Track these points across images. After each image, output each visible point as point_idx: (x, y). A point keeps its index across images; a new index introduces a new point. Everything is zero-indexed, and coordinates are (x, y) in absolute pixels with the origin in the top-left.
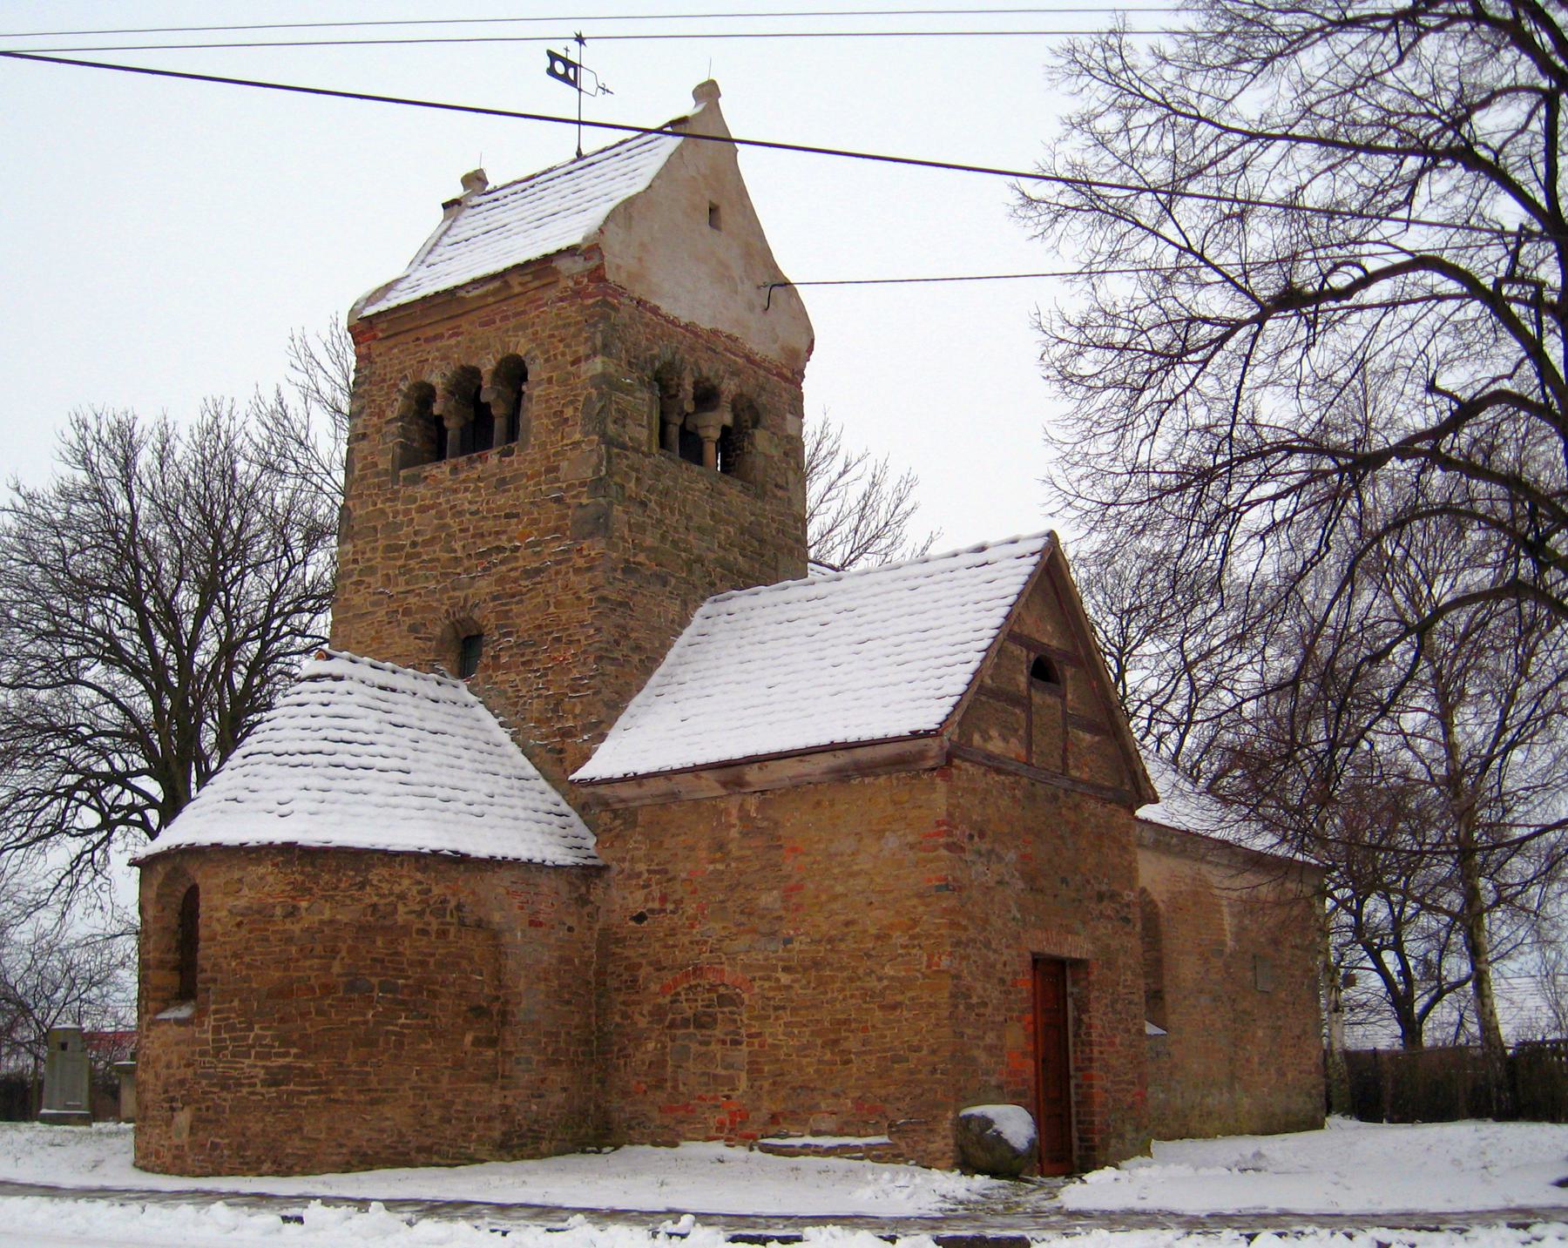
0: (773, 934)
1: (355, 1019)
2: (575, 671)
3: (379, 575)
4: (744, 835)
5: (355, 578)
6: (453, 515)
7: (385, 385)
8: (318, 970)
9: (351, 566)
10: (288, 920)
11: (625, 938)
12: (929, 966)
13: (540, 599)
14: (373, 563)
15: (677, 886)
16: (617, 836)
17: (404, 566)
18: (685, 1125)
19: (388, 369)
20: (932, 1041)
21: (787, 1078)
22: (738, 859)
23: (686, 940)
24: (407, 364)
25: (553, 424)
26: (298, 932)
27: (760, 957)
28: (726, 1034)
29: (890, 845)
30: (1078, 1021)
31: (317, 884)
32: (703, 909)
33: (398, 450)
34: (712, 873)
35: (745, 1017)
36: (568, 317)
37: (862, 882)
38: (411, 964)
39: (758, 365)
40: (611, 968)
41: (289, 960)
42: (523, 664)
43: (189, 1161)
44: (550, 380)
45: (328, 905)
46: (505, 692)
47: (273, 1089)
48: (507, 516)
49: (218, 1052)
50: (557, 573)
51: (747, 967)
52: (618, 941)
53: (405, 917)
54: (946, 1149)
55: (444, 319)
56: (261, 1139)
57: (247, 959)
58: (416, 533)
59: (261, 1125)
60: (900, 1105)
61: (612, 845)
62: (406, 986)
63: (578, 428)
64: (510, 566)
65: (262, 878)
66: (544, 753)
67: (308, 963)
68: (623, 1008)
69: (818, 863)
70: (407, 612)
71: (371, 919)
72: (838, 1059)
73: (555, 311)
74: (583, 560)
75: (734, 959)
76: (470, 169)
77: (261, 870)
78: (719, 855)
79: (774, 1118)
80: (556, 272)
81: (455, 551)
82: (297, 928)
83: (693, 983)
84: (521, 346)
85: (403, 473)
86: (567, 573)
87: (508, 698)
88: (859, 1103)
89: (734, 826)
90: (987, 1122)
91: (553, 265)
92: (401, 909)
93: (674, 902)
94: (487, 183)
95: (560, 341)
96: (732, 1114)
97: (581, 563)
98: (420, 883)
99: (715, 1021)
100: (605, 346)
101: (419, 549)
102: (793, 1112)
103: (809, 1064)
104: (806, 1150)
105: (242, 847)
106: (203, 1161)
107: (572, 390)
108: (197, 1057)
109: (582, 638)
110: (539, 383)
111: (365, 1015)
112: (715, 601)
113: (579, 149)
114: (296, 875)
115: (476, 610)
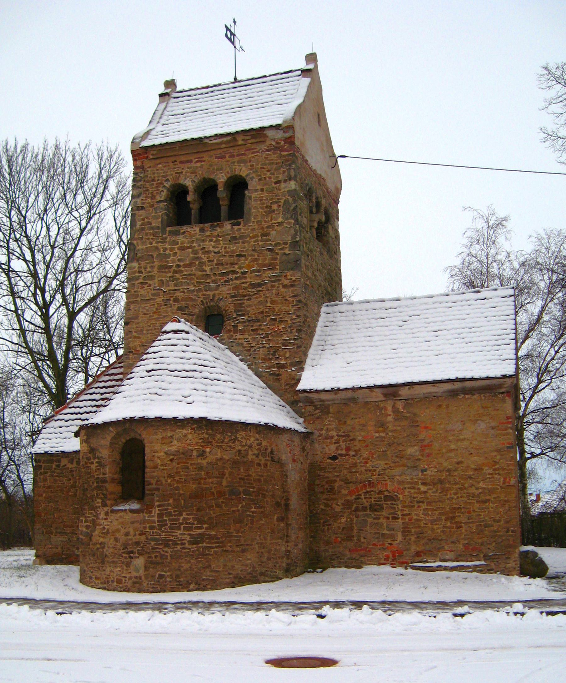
0: (415, 467)
1: (234, 509)
2: (285, 336)
3: (156, 280)
4: (396, 420)
5: (141, 281)
6: (203, 253)
7: (155, 183)
8: (216, 484)
9: (137, 275)
10: (199, 458)
11: (326, 467)
12: (504, 483)
13: (262, 299)
14: (152, 273)
15: (356, 443)
16: (317, 418)
17: (173, 277)
18: (366, 558)
19: (156, 175)
20: (506, 517)
21: (425, 535)
22: (391, 431)
23: (363, 469)
24: (169, 173)
25: (265, 212)
26: (205, 464)
27: (408, 478)
28: (389, 514)
29: (481, 427)
31: (214, 439)
32: (373, 454)
33: (165, 217)
34: (377, 437)
35: (400, 506)
36: (272, 160)
37: (466, 443)
38: (255, 481)
40: (317, 482)
41: (201, 479)
42: (253, 330)
43: (145, 585)
44: (262, 190)
45: (219, 450)
46: (242, 344)
47: (195, 546)
48: (237, 256)
49: (161, 526)
50: (273, 286)
51: (400, 483)
52: (321, 469)
53: (252, 457)
54: (516, 566)
55: (192, 153)
56: (189, 572)
57: (177, 478)
59: (189, 565)
60: (490, 547)
61: (314, 422)
62: (253, 492)
63: (281, 216)
64: (242, 281)
65: (185, 436)
66: (267, 375)
67: (211, 480)
68: (326, 502)
69: (441, 434)
70: (176, 300)
71: (238, 458)
72: (454, 526)
73: (264, 155)
74: (288, 281)
75: (393, 479)
76: (169, 78)
77: (185, 432)
78: (381, 429)
79: (418, 554)
80: (265, 136)
81: (206, 271)
82: (204, 462)
83: (368, 490)
84: (244, 171)
85: (168, 229)
86: (279, 287)
87: (244, 347)
88: (466, 546)
89: (390, 415)
90: (535, 554)
91: (264, 133)
92: (250, 453)
93: (355, 451)
94: (176, 87)
95: (268, 171)
96: (393, 552)
97: (286, 282)
98: (258, 440)
99: (382, 508)
101: (181, 268)
102: (430, 551)
103: (438, 529)
104: (439, 568)
105: (175, 419)
106: (154, 584)
107: (276, 196)
108: (148, 530)
109: (289, 320)
110: (256, 191)
111: (238, 507)
112: (327, 306)
113: (235, 76)
114: (204, 435)
115: (221, 301)
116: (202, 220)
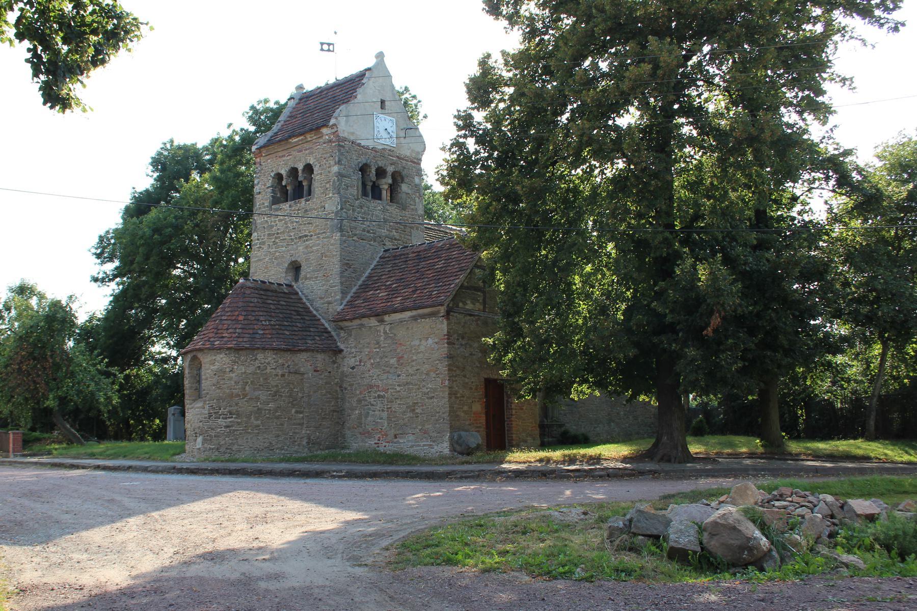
4: (385, 339)
30: (508, 401)
37: (421, 355)
39: (403, 159)
58: (278, 229)
84: (311, 161)
92: (268, 368)
100: (339, 161)
110: (317, 175)
116: (294, 199)
